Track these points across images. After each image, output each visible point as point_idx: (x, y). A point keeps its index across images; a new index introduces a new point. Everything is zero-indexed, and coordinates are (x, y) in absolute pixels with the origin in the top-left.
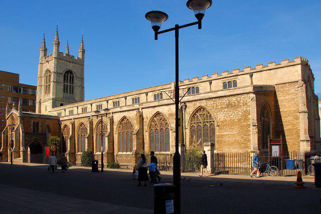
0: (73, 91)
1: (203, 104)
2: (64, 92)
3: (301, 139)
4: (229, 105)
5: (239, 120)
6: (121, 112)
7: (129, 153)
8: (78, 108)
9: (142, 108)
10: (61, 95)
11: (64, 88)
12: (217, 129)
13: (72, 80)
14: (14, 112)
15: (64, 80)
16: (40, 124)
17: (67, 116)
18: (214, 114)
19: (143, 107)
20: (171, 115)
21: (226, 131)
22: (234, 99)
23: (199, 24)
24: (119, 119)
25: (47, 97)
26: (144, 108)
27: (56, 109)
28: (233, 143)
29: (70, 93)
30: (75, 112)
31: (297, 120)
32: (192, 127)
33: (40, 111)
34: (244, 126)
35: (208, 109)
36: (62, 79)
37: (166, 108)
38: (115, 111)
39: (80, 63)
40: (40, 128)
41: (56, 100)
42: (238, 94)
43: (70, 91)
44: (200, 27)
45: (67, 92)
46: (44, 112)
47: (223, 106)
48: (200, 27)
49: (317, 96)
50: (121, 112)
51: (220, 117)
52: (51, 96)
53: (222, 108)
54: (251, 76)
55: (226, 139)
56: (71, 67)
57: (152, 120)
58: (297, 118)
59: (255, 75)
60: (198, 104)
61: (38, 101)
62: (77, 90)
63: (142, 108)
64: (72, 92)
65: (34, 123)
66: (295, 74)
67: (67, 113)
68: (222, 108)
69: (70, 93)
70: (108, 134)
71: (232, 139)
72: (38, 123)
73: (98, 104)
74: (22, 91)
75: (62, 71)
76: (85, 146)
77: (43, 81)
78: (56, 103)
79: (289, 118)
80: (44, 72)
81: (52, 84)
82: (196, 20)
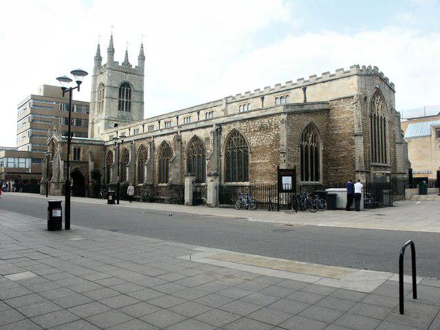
0: (130, 109)
1: (237, 126)
2: (119, 109)
3: (357, 169)
4: (262, 128)
5: (271, 145)
6: (161, 135)
7: (164, 184)
8: (198, 113)
9: (181, 132)
10: (115, 113)
11: (119, 105)
12: (250, 156)
13: (129, 95)
14: (55, 137)
15: (120, 95)
16: (81, 151)
17: (146, 133)
18: (246, 136)
19: (181, 129)
20: (208, 139)
21: (258, 159)
22: (266, 120)
23: (78, 87)
24: (159, 144)
25: (100, 116)
26: (156, 136)
27: (109, 131)
28: (265, 173)
29: (126, 111)
30: (141, 131)
31: (352, 144)
32: (227, 154)
33: (92, 136)
34: (275, 152)
35: (241, 132)
36: (116, 95)
37: (203, 131)
38: (155, 135)
39: (139, 72)
40: (81, 155)
41: (109, 120)
42: (270, 115)
43: (126, 109)
44: (79, 90)
45: (123, 110)
46: (97, 137)
47: (256, 129)
48: (79, 90)
49: (399, 113)
50: (161, 135)
51: (253, 141)
52: (103, 116)
53: (255, 131)
54: (305, 90)
55: (258, 168)
56: (127, 78)
57: (190, 143)
58: (352, 143)
59: (309, 89)
60: (233, 127)
61: (90, 121)
62: (134, 107)
63: (181, 132)
64: (128, 108)
65: (75, 149)
66: (351, 87)
67: (132, 133)
68: (255, 131)
69: (126, 111)
70: (147, 161)
71: (264, 169)
72: (79, 150)
73: (150, 124)
74: (75, 109)
75: (117, 84)
76: (125, 175)
77: (97, 97)
78: (113, 123)
79: (344, 142)
80: (98, 86)
81: (105, 100)
82: (77, 85)
